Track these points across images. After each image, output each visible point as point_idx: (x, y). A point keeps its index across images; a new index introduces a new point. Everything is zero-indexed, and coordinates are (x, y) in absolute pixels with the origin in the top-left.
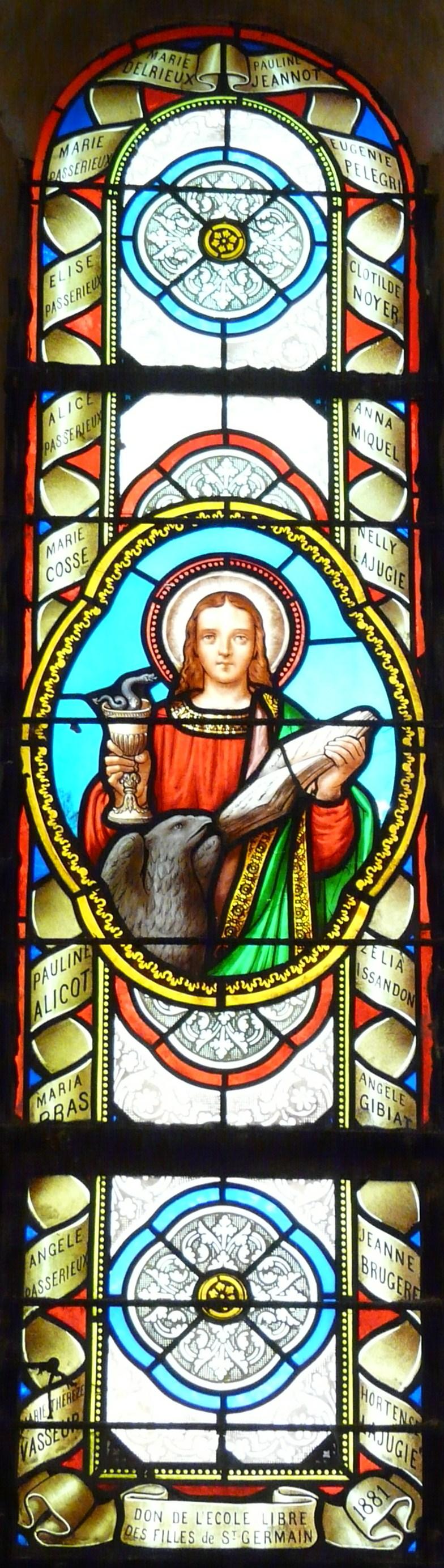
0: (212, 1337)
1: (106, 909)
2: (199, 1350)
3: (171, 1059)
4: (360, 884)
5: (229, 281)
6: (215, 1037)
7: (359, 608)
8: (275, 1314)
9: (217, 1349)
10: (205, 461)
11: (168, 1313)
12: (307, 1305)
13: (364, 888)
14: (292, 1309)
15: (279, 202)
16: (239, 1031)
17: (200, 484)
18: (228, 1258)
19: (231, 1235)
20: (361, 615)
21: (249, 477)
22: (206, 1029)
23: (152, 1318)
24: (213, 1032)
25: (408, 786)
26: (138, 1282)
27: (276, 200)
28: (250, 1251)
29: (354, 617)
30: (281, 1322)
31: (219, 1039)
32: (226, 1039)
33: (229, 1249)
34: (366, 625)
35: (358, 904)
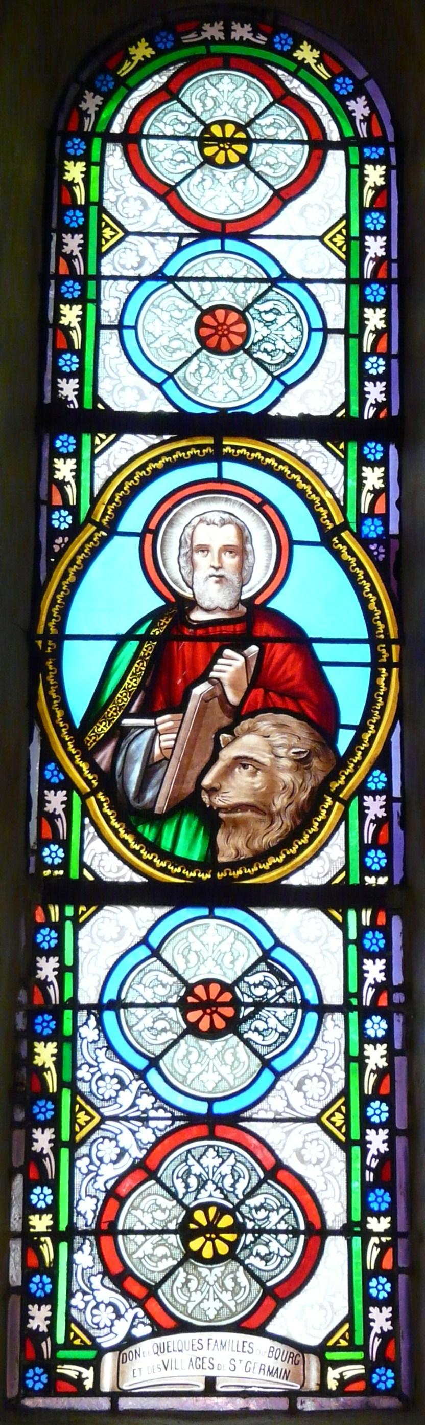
3: (262, 1154)
8: (174, 130)
9: (216, 377)
11: (277, 133)
12: (148, 137)
14: (161, 134)
15: (162, 1175)
18: (208, 1052)
19: (204, 1073)
22: (207, 376)
23: (290, 130)
26: (301, 343)
30: (147, 1212)
32: (214, 1299)
33: (216, 374)
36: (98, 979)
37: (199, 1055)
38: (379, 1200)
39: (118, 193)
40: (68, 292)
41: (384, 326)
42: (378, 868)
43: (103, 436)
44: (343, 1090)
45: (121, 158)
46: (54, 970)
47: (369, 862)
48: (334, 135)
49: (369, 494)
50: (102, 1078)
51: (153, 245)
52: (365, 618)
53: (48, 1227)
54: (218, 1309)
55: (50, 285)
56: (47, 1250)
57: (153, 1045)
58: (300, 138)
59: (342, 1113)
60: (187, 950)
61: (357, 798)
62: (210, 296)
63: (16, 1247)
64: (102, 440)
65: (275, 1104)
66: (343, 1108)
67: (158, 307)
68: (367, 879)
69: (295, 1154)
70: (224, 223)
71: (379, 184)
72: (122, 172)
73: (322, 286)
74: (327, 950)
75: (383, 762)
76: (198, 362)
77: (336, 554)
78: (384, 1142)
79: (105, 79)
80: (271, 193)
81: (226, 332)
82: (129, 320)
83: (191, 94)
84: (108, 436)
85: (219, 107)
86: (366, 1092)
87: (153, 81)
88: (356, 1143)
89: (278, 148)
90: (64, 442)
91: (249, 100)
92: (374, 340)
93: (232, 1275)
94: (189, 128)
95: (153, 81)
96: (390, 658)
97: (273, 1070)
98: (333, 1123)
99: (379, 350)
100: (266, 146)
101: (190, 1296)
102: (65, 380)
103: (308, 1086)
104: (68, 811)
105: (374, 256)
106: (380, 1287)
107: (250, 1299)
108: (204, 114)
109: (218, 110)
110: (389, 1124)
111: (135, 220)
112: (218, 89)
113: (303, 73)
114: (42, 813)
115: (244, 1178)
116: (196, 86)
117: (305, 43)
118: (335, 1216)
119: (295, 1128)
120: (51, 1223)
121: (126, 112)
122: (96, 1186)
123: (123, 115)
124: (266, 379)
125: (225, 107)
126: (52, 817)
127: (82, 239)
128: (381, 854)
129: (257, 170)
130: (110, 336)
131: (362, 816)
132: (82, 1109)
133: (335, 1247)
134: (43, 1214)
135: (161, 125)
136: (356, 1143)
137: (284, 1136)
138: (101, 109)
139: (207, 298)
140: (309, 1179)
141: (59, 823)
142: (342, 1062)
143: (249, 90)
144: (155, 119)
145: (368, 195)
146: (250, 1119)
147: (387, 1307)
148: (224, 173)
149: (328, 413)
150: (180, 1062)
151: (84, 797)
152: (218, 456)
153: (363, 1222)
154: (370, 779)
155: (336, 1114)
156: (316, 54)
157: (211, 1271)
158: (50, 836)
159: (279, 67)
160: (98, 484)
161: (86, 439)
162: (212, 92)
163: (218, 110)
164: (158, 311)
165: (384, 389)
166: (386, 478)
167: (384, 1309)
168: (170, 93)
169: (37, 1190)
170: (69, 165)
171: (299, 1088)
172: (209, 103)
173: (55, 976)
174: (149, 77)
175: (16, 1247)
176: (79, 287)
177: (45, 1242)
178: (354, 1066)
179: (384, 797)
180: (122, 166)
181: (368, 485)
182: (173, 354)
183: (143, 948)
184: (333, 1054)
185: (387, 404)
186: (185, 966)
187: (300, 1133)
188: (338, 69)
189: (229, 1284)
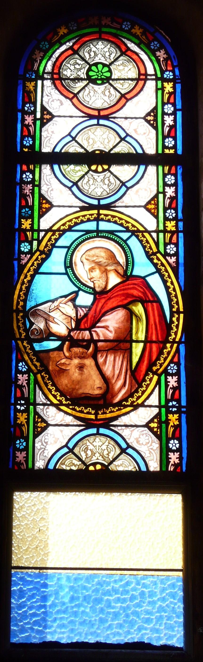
0: (95, 181)
1: (48, 379)
2: (90, 185)
4: (154, 368)
5: (101, 183)
7: (154, 254)
9: (97, 185)
11: (75, 168)
13: (156, 370)
20: (155, 257)
22: (92, 185)
25: (175, 327)
27: (120, 183)
29: (152, 258)
34: (158, 261)
35: (153, 376)
36: (50, 149)
38: (171, 214)
39: (48, 187)
41: (173, 91)
42: (172, 218)
45: (50, 170)
47: (167, 215)
48: (150, 70)
50: (53, 101)
51: (62, 431)
61: (164, 374)
65: (126, 200)
71: (170, 91)
73: (147, 401)
74: (151, 449)
79: (44, 44)
81: (100, 72)
85: (94, 455)
92: (169, 130)
94: (82, 66)
96: (178, 309)
97: (126, 186)
99: (173, 241)
102: (19, 452)
105: (168, 92)
108: (90, 60)
109: (96, 57)
111: (57, 110)
112: (96, 48)
114: (23, 125)
115: (113, 451)
125: (99, 180)
126: (28, 126)
128: (176, 442)
139: (92, 60)
141: (31, 128)
145: (167, 130)
146: (114, 118)
150: (85, 184)
151: (35, 375)
154: (169, 368)
158: (27, 134)
159: (125, 38)
162: (94, 49)
163: (96, 57)
167: (174, 377)
172: (92, 54)
178: (160, 92)
182: (77, 173)
183: (69, 137)
185: (180, 464)
186: (87, 145)
187: (138, 431)
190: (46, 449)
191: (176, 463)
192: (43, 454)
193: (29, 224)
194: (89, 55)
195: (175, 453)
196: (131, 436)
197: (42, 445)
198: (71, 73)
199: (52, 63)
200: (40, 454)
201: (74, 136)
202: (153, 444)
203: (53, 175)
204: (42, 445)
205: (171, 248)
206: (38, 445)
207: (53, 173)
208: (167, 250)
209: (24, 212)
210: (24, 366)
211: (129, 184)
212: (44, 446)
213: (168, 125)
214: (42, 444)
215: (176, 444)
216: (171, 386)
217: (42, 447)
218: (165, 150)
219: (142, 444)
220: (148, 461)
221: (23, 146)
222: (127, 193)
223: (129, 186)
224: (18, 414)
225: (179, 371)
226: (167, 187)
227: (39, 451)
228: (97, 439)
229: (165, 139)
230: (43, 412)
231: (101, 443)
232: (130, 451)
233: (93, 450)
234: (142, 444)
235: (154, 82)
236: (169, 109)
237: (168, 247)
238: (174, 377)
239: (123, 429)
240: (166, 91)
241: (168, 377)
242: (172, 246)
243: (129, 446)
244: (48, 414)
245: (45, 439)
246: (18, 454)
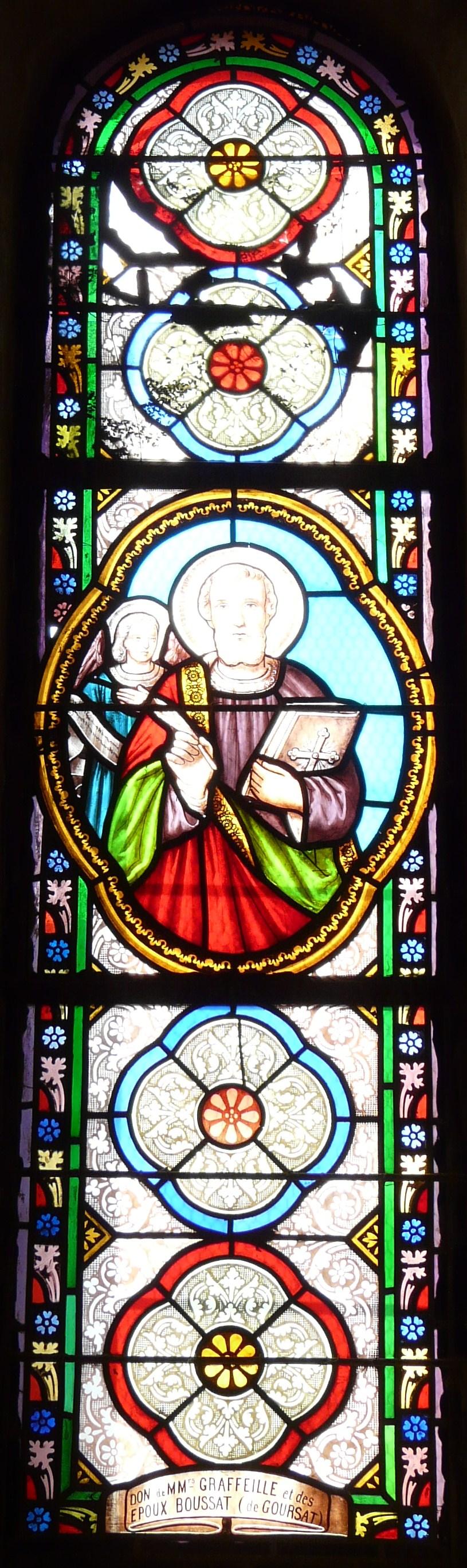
6: (219, 1433)
10: (214, 93)
11: (293, 1348)
14: (165, 155)
16: (244, 1426)
17: (210, 115)
21: (257, 1046)
24: (217, 1427)
28: (257, 1304)
31: (223, 1435)
32: (230, 1435)
37: (214, 1415)
38: (410, 1043)
40: (61, 503)
42: (405, 509)
43: (106, 491)
44: (377, 1207)
46: (60, 1072)
49: (400, 547)
52: (401, 770)
53: (58, 1166)
54: (233, 1446)
55: (32, 801)
56: (55, 1188)
57: (166, 1154)
58: (322, 1356)
59: (374, 1233)
60: (211, 113)
62: (219, 130)
63: (26, 1182)
64: (105, 497)
65: (300, 1223)
66: (376, 1228)
67: (156, 1086)
68: (402, 970)
69: (321, 1275)
70: (231, 1255)
71: (406, 291)
72: (100, 1404)
75: (419, 841)
76: (211, 201)
77: (364, 610)
78: (419, 1077)
80: (288, 216)
81: (237, 370)
82: (122, 1106)
83: (197, 112)
84: (111, 492)
86: (402, 1211)
87: (157, 96)
88: (389, 1362)
89: (294, 1368)
90: (65, 499)
91: (260, 117)
93: (251, 1410)
95: (157, 96)
96: (424, 726)
98: (365, 1244)
100: (279, 1366)
101: (204, 1429)
102: (38, 1442)
103: (337, 1452)
104: (73, 902)
106: (413, 1136)
107: (269, 1437)
108: (211, 133)
110: (425, 1243)
113: (325, 90)
114: (32, 1273)
116: (202, 103)
117: (329, 58)
118: (365, 1342)
119: (319, 1248)
120: (61, 1161)
121: (127, 130)
122: (106, 1309)
123: (125, 134)
124: (284, 216)
125: (234, 125)
127: (79, 431)
129: (273, 393)
130: (113, 377)
131: (397, 900)
132: (91, 1225)
133: (366, 1382)
134: (68, 517)
135: (164, 146)
136: (389, 1362)
137: (309, 1255)
138: (100, 128)
140: (336, 1059)
141: (64, 916)
142: (375, 1425)
143: (261, 106)
144: (159, 139)
147: (421, 1251)
148: (230, 1155)
149: (356, 972)
152: (233, 514)
153: (398, 1353)
155: (369, 1234)
156: (341, 69)
157: (230, 1318)
160: (102, 549)
161: (88, 494)
162: (220, 109)
164: (156, 1091)
165: (422, 887)
166: (418, 530)
168: (172, 111)
169: (50, 1030)
170: (35, 1446)
171: (325, 1455)
173: (74, 538)
174: (154, 92)
175: (26, 1182)
176: (74, 498)
177: (55, 1181)
178: (388, 1094)
179: (413, 349)
180: (101, 1395)
181: (399, 538)
183: (158, 1049)
184: (365, 1416)
185: (415, 294)
187: (327, 1252)
188: (365, 86)
189: (247, 1419)
190: (112, 1052)
191: (418, 1087)
192: (103, 1307)
193: (72, 531)
194: (201, 1306)
195: (415, 1064)
196: (310, 1264)
197: (99, 1284)
198: (162, 1113)
199: (124, 139)
200: (96, 1308)
201: (171, 1047)
202: (364, 1284)
203: (114, 1151)
204: (99, 1284)
205: (402, 409)
206: (94, 1044)
207: (115, 1147)
208: (401, 1047)
209: (42, 1516)
210: (63, 860)
211: (308, 420)
212: (107, 1045)
213: (402, 541)
214: (101, 1284)
215: (413, 1041)
216: (410, 1473)
217: (103, 1047)
218: (404, 1351)
219: (338, 1283)
220: (352, 1326)
221: (46, 962)
222: (303, 1204)
223: (309, 424)
224: (58, 427)
225: (427, 955)
226: (407, 1348)
227: (93, 1300)
228: (236, 440)
229: (393, 405)
230: (100, 1204)
231: (242, 103)
232: (308, 1057)
233: (221, 1297)
234: (338, 1283)
235: (363, 170)
236: (402, 253)
237: (397, 407)
238: (418, 1449)
239: (293, 1248)
240: (407, 1086)
241: (404, 1450)
242: (406, 405)
243: (307, 1045)
244: (111, 1208)
245: (108, 1269)
246: (59, 522)
